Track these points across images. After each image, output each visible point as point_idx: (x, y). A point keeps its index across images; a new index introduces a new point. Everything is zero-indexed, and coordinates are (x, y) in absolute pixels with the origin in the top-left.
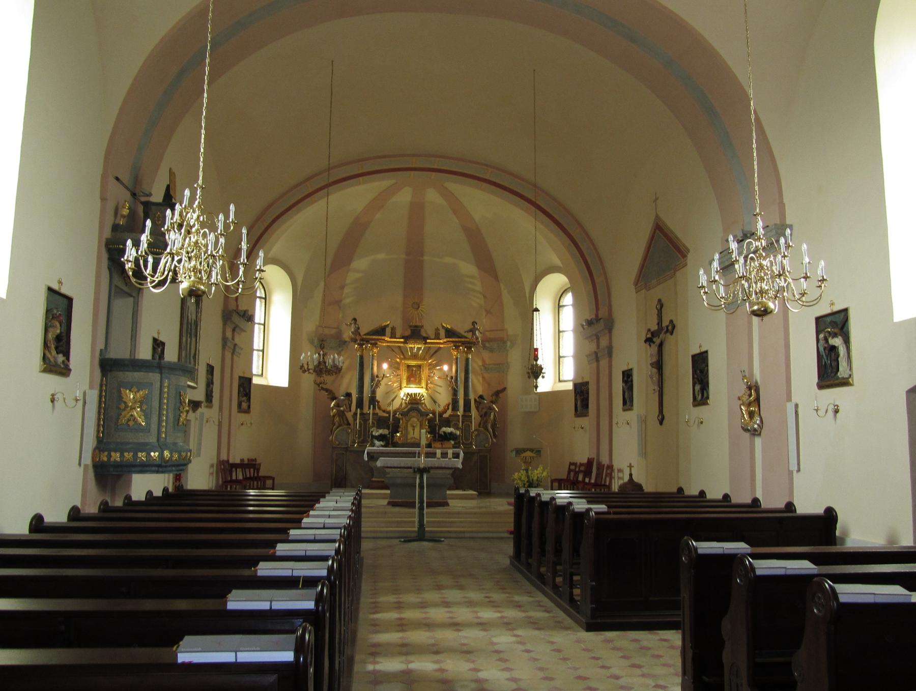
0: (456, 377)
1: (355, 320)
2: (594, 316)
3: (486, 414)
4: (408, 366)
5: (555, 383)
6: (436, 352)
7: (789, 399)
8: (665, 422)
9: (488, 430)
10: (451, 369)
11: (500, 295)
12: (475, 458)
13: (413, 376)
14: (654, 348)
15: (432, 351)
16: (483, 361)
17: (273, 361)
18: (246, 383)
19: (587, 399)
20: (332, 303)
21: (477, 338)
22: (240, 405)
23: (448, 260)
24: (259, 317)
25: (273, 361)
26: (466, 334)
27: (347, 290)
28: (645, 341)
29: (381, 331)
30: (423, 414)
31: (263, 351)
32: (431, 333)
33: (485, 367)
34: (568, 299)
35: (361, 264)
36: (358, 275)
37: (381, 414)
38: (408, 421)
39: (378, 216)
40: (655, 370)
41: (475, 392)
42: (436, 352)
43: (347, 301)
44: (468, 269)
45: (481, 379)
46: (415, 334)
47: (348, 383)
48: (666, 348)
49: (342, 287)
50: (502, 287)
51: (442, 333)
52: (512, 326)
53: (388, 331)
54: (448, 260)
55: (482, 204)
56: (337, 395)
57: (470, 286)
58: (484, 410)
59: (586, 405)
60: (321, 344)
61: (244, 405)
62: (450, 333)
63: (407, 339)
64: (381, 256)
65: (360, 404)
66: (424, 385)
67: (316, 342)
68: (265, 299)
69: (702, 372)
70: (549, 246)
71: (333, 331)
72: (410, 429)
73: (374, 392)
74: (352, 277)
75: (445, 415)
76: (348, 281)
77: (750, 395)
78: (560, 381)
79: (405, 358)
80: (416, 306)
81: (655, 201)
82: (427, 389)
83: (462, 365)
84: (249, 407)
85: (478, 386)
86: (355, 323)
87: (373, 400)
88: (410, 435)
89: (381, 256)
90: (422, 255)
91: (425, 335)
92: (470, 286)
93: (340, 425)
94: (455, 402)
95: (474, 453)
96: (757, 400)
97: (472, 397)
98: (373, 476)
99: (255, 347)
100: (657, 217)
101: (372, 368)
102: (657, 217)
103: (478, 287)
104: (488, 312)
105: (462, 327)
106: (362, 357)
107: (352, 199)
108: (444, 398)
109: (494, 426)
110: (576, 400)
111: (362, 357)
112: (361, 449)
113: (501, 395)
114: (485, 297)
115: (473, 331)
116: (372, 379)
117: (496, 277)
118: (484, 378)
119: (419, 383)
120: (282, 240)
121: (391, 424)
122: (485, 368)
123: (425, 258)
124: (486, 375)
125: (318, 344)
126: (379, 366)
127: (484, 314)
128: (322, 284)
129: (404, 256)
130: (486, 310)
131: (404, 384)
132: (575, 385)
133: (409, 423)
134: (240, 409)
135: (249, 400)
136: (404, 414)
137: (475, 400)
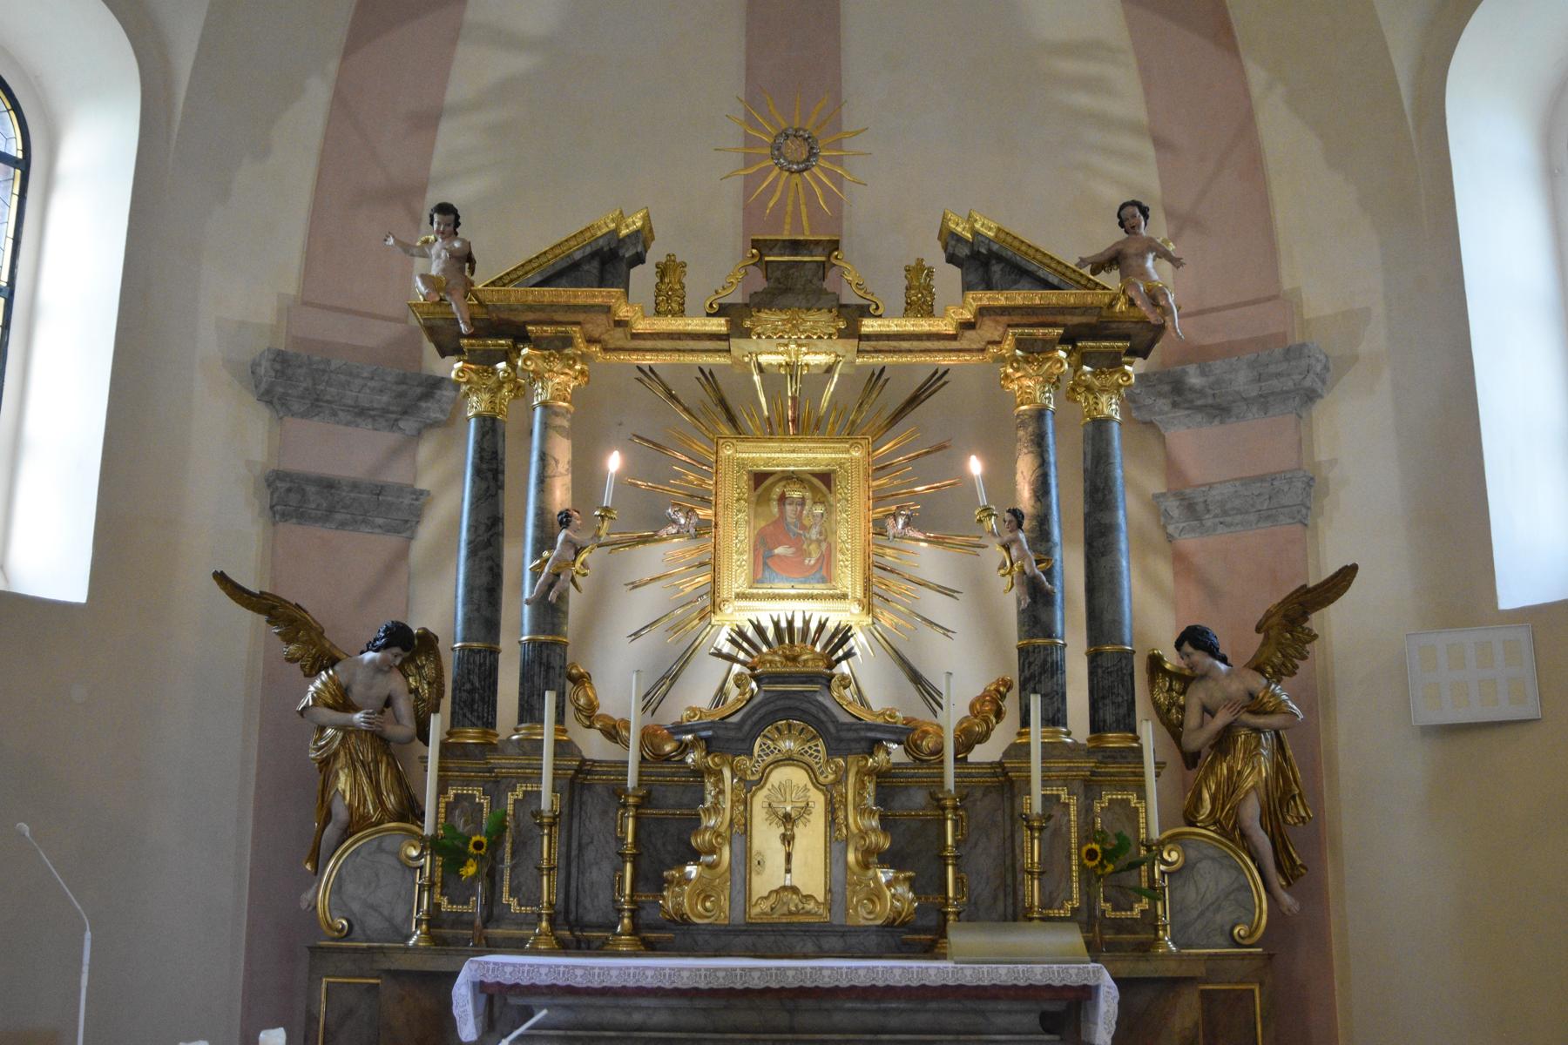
0: (1043, 520)
3: (1223, 742)
4: (759, 478)
6: (914, 401)
9: (1244, 840)
10: (1001, 474)
13: (784, 548)
15: (897, 394)
16: (1172, 469)
20: (367, 183)
21: (1154, 297)
29: (609, 260)
30: (851, 738)
32: (893, 290)
36: (517, 63)
37: (593, 745)
38: (750, 786)
42: (914, 401)
45: (1164, 570)
46: (792, 274)
49: (428, 120)
50: (1257, 75)
51: (948, 277)
53: (642, 278)
56: (335, 637)
57: (1082, 100)
58: (1222, 719)
60: (290, 381)
62: (984, 262)
63: (736, 318)
65: (476, 697)
66: (848, 578)
68: (24, 165)
72: (766, 837)
74: (475, 70)
75: (985, 753)
76: (459, 89)
82: (869, 608)
87: (551, 668)
91: (850, 297)
92: (1082, 100)
94: (1038, 669)
95: (1174, 983)
101: (543, 480)
103: (1129, 102)
105: (1070, 236)
106: (490, 427)
108: (965, 668)
109: (1273, 816)
112: (441, 964)
113: (1315, 621)
114: (1160, 143)
116: (544, 541)
118: (1180, 560)
119: (824, 570)
121: (663, 805)
122: (1191, 509)
128: (318, 94)
131: (736, 577)
133: (759, 800)
136: (727, 737)
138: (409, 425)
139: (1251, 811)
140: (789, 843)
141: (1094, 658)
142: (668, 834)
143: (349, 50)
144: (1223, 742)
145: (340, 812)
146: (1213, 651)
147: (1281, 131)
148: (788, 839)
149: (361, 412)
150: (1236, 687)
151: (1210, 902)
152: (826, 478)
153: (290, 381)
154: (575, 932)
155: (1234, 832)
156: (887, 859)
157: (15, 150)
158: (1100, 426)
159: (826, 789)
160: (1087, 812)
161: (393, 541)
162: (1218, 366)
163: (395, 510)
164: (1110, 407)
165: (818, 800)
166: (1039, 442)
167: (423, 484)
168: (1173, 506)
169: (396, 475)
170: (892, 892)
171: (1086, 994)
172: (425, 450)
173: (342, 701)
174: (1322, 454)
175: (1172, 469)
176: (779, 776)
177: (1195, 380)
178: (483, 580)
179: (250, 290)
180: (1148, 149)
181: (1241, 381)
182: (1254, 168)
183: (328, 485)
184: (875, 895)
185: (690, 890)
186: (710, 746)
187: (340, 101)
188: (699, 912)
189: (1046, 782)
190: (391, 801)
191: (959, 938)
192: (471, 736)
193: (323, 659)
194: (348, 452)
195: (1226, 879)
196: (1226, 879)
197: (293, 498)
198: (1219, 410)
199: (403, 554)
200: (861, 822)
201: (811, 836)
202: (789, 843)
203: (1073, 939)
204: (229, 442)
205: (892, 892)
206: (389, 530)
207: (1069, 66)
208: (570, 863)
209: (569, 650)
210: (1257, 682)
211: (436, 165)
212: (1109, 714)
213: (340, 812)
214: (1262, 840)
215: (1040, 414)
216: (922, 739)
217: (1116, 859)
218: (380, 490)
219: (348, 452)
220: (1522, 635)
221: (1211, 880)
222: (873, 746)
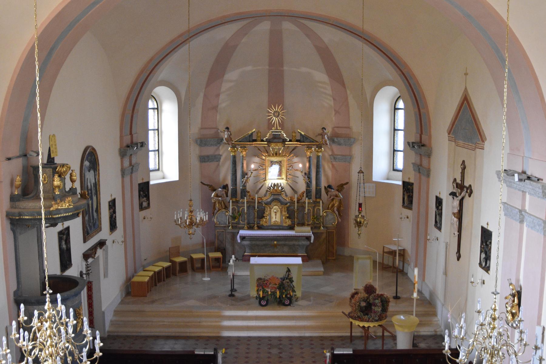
1: (227, 128)
2: (418, 140)
5: (390, 171)
6: (293, 150)
7: (539, 323)
8: (460, 259)
10: (304, 165)
11: (347, 98)
12: (324, 236)
14: (456, 203)
16: (332, 151)
17: (166, 163)
18: (144, 189)
19: (412, 197)
20: (210, 107)
22: (141, 205)
23: (304, 70)
24: (152, 144)
25: (166, 163)
26: (317, 139)
27: (222, 97)
28: (450, 194)
31: (158, 130)
33: (334, 157)
34: (401, 104)
35: (232, 75)
38: (271, 209)
39: (243, 40)
40: (456, 220)
41: (326, 176)
42: (293, 150)
43: (223, 105)
44: (321, 76)
45: (331, 166)
47: (224, 174)
48: (465, 202)
49: (218, 95)
50: (348, 92)
52: (356, 126)
54: (304, 70)
55: (328, 35)
57: (322, 90)
58: (332, 198)
59: (411, 202)
60: (202, 142)
61: (145, 204)
64: (249, 68)
67: (199, 141)
68: (157, 109)
69: (487, 245)
70: (387, 70)
71: (212, 132)
72: (273, 215)
73: (244, 186)
74: (225, 86)
76: (223, 89)
77: (514, 301)
78: (394, 170)
79: (269, 156)
80: (277, 114)
81: (466, 74)
83: (314, 161)
84: (149, 204)
85: (328, 175)
86: (228, 131)
87: (244, 192)
88: (273, 220)
89: (249, 68)
90: (282, 67)
92: (322, 90)
93: (219, 210)
96: (519, 305)
97: (323, 184)
98: (245, 252)
99: (151, 126)
100: (466, 89)
102: (466, 89)
103: (329, 91)
104: (337, 112)
106: (234, 157)
107: (225, 33)
110: (404, 194)
111: (234, 157)
113: (345, 186)
114: (334, 99)
115: (322, 135)
117: (343, 84)
118: (333, 165)
120: (164, 72)
122: (335, 158)
123: (285, 68)
124: (334, 163)
125: (199, 143)
126: (248, 165)
127: (334, 113)
128: (202, 95)
129: (268, 67)
130: (335, 110)
132: (404, 182)
133: (272, 210)
134: (141, 208)
135: (148, 199)
137: (325, 187)
138: (218, 145)
139: (335, 209)
140: (275, 215)
141: (316, 189)
142: (261, 215)
143: (206, 88)
144: (333, 200)
145: (217, 209)
146: (332, 189)
147: (352, 102)
148: (276, 215)
149: (211, 145)
150: (334, 193)
151: (331, 220)
152: (281, 162)
153: (202, 142)
154: (251, 228)
155: (334, 211)
156: (288, 217)
157: (156, 107)
158: (318, 157)
159: (281, 209)
160: (314, 210)
161: (216, 163)
162: (339, 139)
163: (216, 158)
164: (320, 154)
165: (279, 210)
166: (310, 162)
167: (221, 154)
168: (332, 157)
169: (217, 153)
170: (288, 222)
171: (310, 237)
172: (220, 148)
173: (217, 196)
174: (353, 153)
175: (332, 151)
176: (274, 207)
177: (336, 140)
178: (234, 179)
179: (194, 130)
180: (332, 99)
181: (342, 142)
182: (347, 106)
183: (208, 156)
184: (286, 223)
185: (263, 222)
186: (266, 204)
187: (205, 96)
188: (265, 225)
189: (308, 207)
190: (223, 207)
191: (297, 228)
192: (234, 200)
193: (214, 190)
194: (210, 151)
195: (332, 217)
196: (332, 217)
197: (203, 159)
198: (340, 144)
199: (218, 165)
200: (285, 214)
201: (278, 214)
202: (275, 215)
203: (309, 229)
204: (194, 151)
205: (288, 222)
206: (217, 161)
207: (320, 85)
208: (249, 216)
209: (93, 283)
210: (337, 193)
211: (220, 102)
212: (317, 196)
213: (217, 209)
214: (337, 213)
215: (310, 157)
216: (270, 284)
217: (317, 217)
218: (215, 156)
219: (210, 151)
220: (374, 185)
221: (330, 217)
222: (286, 204)
